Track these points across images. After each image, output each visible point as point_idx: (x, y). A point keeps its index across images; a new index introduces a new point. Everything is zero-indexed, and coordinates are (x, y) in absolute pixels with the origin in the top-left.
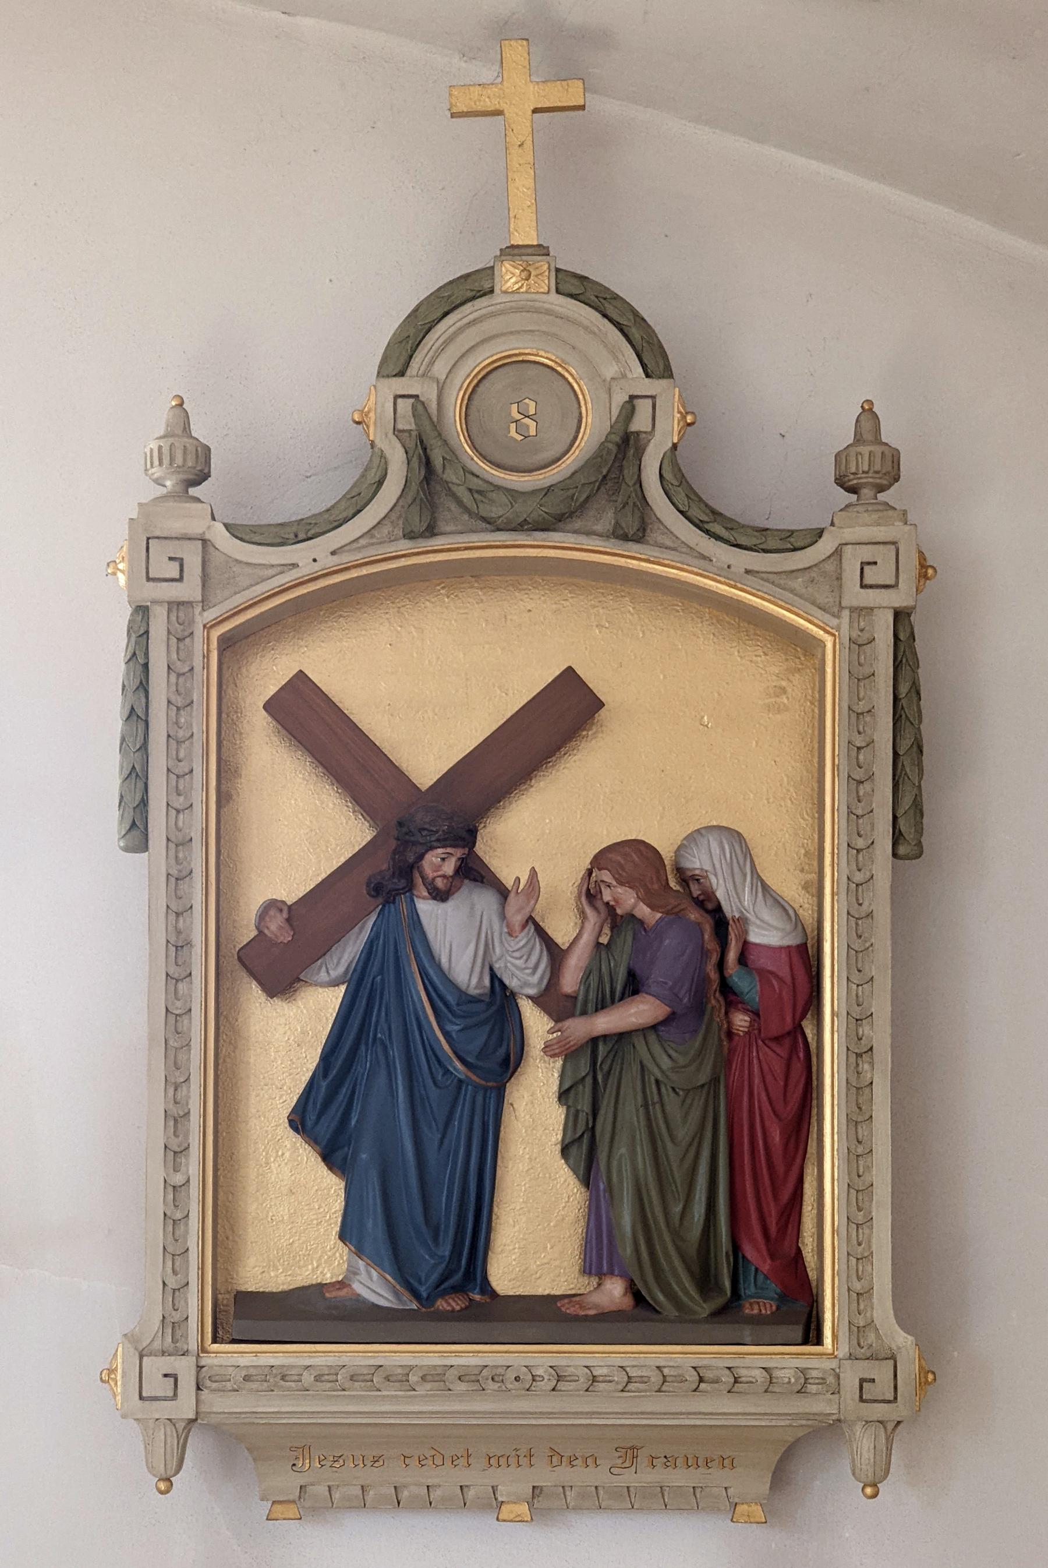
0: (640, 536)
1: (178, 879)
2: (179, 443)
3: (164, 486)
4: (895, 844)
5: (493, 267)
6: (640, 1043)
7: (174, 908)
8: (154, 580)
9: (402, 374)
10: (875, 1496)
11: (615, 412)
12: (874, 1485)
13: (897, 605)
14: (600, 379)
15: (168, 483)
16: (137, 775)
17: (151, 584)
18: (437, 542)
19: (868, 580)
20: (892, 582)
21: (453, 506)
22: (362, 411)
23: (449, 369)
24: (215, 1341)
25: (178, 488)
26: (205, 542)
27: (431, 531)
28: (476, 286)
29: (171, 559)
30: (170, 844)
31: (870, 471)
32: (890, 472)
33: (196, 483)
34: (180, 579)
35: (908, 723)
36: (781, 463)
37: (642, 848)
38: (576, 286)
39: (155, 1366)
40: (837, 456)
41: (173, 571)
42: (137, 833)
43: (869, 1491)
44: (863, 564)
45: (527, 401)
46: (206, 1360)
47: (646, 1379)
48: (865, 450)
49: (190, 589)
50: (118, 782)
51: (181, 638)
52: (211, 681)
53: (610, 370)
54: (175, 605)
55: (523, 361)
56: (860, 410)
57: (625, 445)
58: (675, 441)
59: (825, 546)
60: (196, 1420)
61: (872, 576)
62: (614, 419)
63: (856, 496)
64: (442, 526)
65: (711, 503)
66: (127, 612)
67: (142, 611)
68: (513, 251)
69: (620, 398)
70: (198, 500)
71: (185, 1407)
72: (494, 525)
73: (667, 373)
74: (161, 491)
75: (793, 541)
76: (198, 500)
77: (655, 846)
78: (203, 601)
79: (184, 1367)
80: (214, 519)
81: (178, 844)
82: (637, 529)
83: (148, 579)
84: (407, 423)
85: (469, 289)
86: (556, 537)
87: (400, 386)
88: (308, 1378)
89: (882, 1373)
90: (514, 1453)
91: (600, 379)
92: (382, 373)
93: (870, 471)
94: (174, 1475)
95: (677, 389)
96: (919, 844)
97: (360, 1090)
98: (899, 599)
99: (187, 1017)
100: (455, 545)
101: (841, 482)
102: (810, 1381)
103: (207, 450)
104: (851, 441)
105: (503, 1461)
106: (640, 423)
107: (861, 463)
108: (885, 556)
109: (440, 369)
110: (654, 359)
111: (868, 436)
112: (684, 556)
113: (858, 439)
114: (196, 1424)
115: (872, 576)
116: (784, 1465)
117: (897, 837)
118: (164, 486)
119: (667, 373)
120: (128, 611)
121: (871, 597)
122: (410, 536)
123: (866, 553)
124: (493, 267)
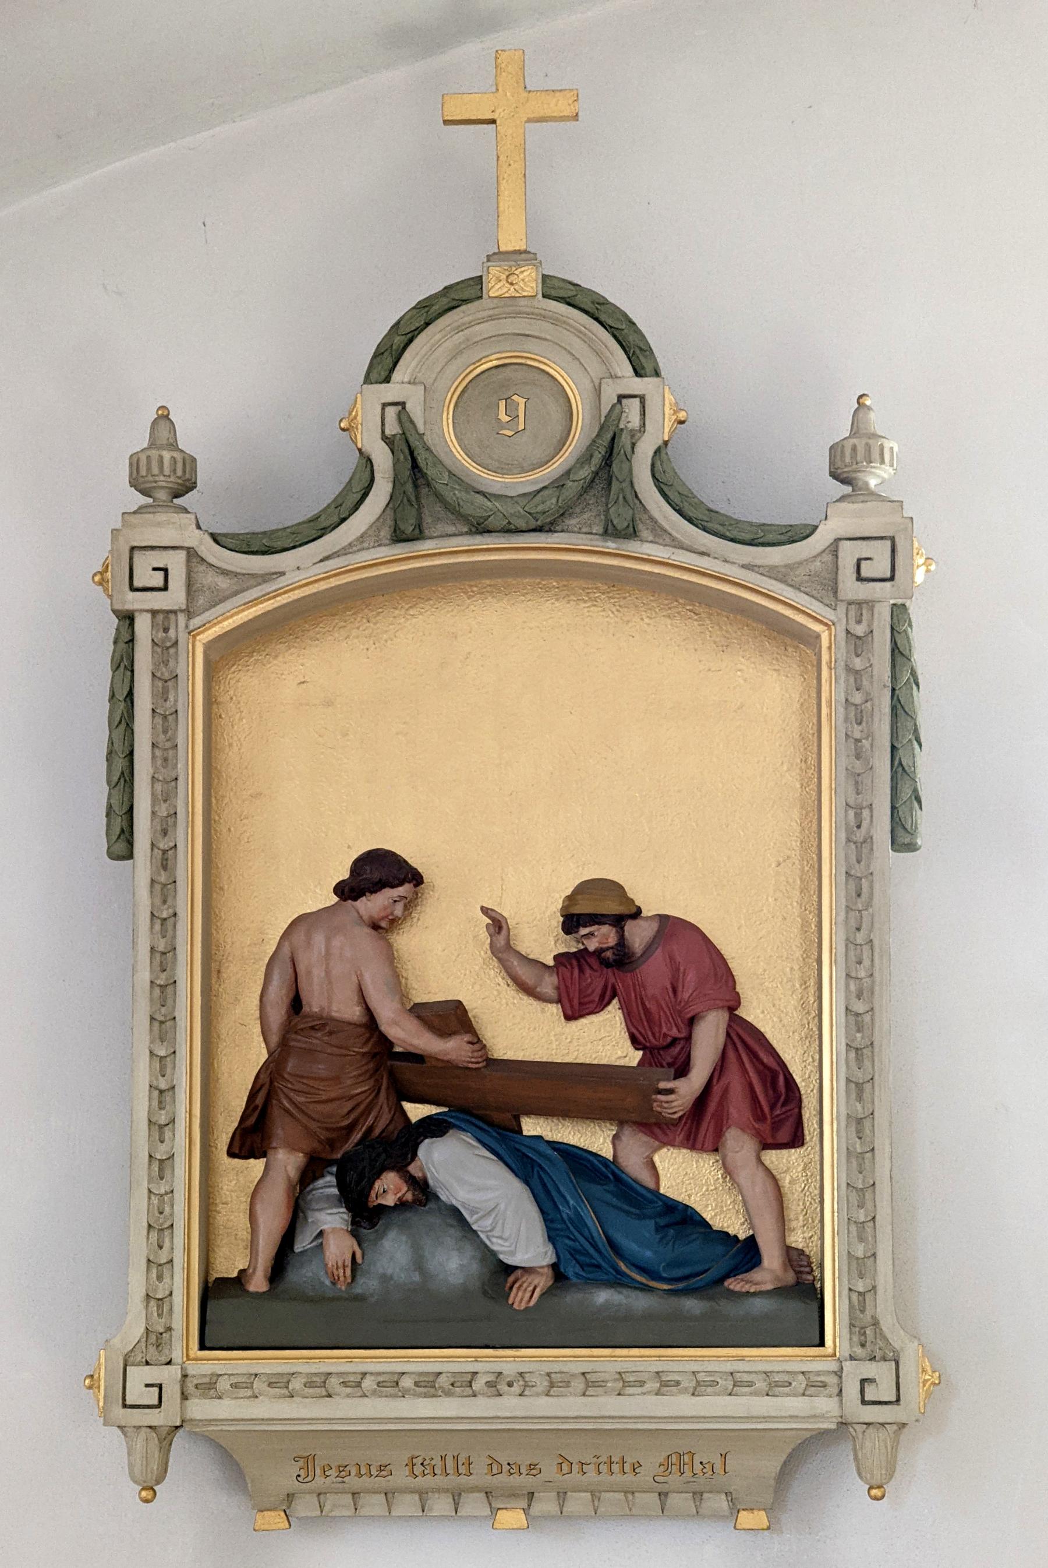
0: (631, 533)
1: (164, 889)
7: (161, 948)
14: (579, 373)
16: (125, 780)
18: (426, 546)
19: (864, 573)
21: (438, 508)
24: (203, 1347)
27: (418, 535)
29: (154, 569)
30: (156, 850)
34: (165, 588)
37: (714, 955)
39: (138, 1376)
40: (831, 448)
41: (158, 580)
42: (122, 842)
45: (515, 397)
49: (176, 597)
52: (195, 900)
54: (162, 618)
55: (543, 371)
56: (856, 406)
57: (610, 451)
58: (666, 438)
60: (181, 1426)
63: (850, 489)
68: (498, 256)
70: (186, 511)
73: (657, 374)
76: (186, 511)
77: (727, 950)
79: (168, 1376)
80: (199, 527)
81: (165, 860)
91: (579, 373)
92: (367, 380)
94: (158, 1483)
99: (171, 1093)
100: (444, 548)
103: (194, 460)
108: (880, 552)
110: (641, 359)
112: (672, 549)
113: (152, 445)
114: (181, 1431)
116: (784, 1474)
121: (864, 591)
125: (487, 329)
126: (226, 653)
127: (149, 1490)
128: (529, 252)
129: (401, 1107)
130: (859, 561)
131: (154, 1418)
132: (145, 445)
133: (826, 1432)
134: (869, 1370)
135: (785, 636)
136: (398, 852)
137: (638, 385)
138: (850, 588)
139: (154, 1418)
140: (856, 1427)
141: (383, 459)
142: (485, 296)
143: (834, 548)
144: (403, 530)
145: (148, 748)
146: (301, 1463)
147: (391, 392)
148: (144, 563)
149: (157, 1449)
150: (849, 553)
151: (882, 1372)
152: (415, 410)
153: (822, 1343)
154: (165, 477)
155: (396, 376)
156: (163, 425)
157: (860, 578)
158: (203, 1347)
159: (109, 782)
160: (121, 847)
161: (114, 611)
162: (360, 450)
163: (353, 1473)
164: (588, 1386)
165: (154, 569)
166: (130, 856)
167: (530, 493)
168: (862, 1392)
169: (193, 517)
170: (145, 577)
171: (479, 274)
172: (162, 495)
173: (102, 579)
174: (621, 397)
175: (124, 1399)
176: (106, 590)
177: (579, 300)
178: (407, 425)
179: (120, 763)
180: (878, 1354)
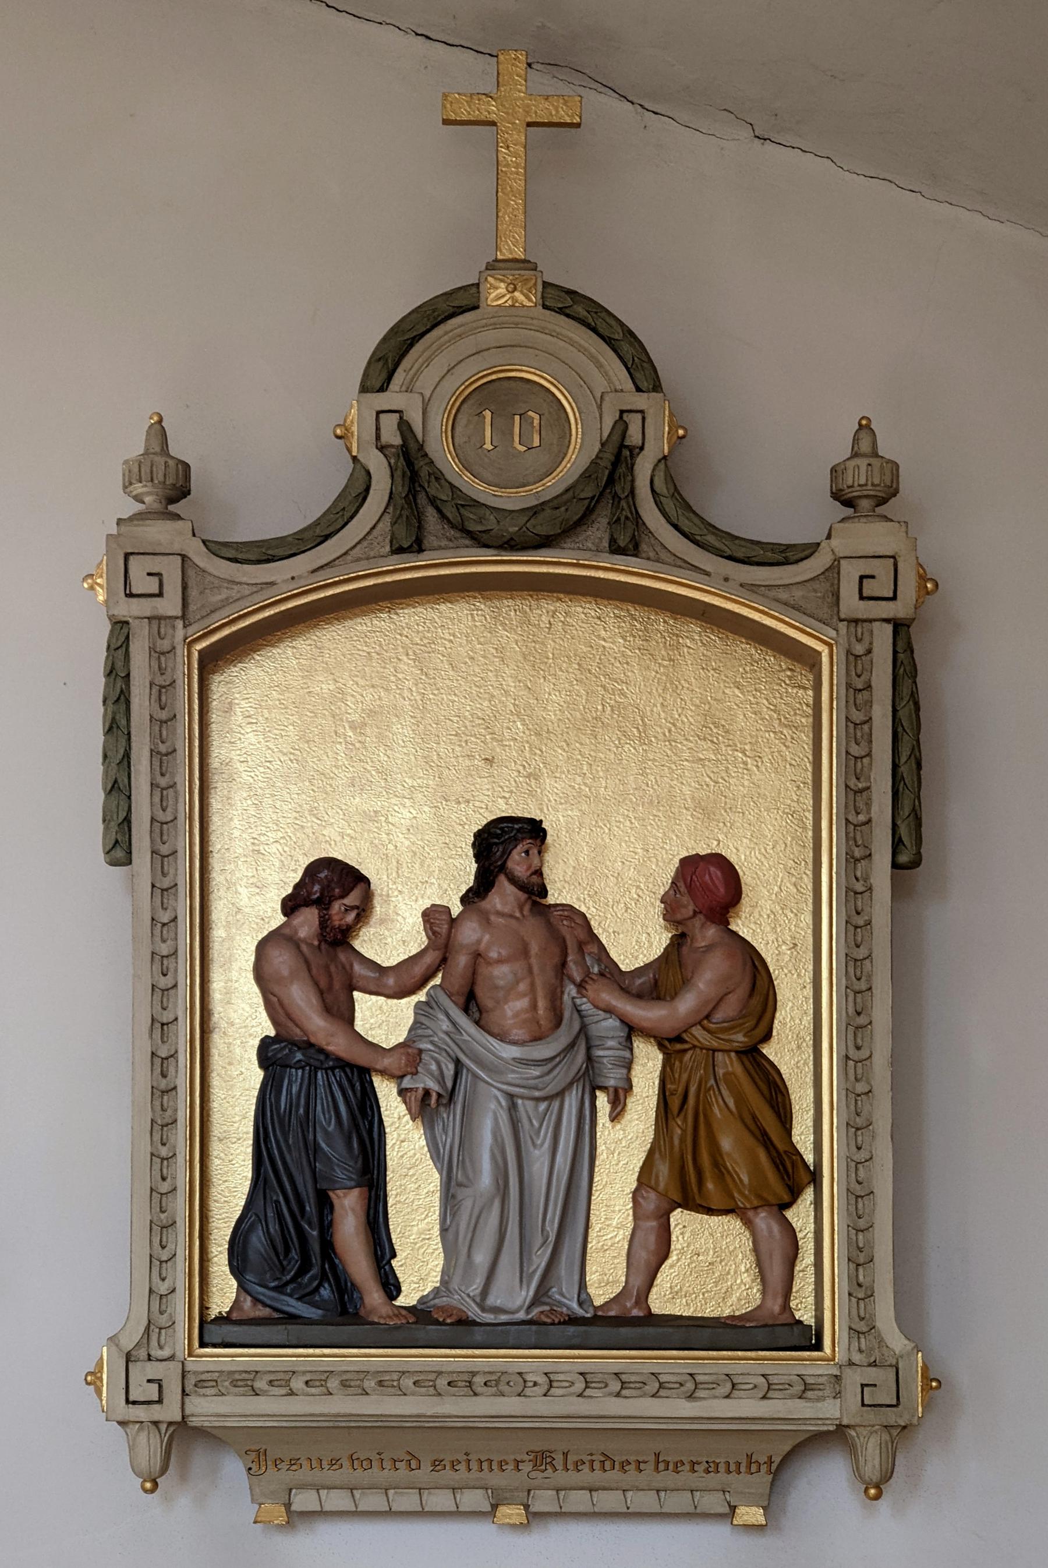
0: (633, 549)
2: (160, 460)
3: (143, 503)
4: (894, 854)
5: (478, 285)
6: (625, 1071)
9: (382, 389)
10: (877, 1497)
12: (877, 1487)
14: (582, 398)
15: (148, 499)
20: (894, 1402)
22: (344, 425)
23: (436, 379)
24: (202, 1345)
25: (157, 506)
26: (184, 557)
27: (418, 547)
28: (456, 303)
29: (149, 574)
31: (866, 490)
32: (886, 494)
33: (172, 500)
36: (771, 489)
38: (569, 304)
40: (834, 470)
41: (153, 586)
42: (119, 849)
43: (872, 1491)
44: (862, 578)
46: (192, 1364)
48: (863, 463)
49: (170, 605)
50: (102, 795)
51: (160, 655)
53: (600, 384)
54: (155, 619)
61: (869, 588)
62: (605, 435)
64: (430, 540)
66: (105, 628)
67: (121, 628)
71: (170, 1411)
72: (480, 540)
73: (657, 387)
74: (139, 507)
75: (786, 555)
78: (183, 617)
79: (170, 1374)
80: (194, 535)
81: (162, 858)
82: (629, 542)
83: (378, 413)
84: (391, 436)
85: (459, 303)
86: (544, 551)
87: (383, 401)
89: (883, 1377)
92: (364, 389)
93: (866, 490)
96: (919, 853)
97: (159, 1446)
98: (898, 610)
101: (836, 495)
103: (187, 467)
104: (848, 455)
105: (485, 1465)
106: (634, 436)
107: (859, 475)
108: (882, 570)
109: (426, 381)
110: (643, 371)
113: (855, 455)
115: (869, 588)
117: (897, 844)
118: (143, 503)
120: (107, 627)
122: (398, 550)
124: (478, 285)
125: (491, 337)
126: (212, 661)
128: (529, 261)
130: (862, 578)
131: (156, 1413)
133: (829, 1432)
134: (872, 1375)
136: (340, 858)
137: (641, 401)
138: (850, 603)
139: (156, 1413)
141: (377, 465)
142: (482, 304)
143: (834, 569)
145: (146, 753)
147: (391, 399)
148: (138, 568)
149: (178, 1444)
150: (850, 572)
152: (415, 418)
156: (864, 436)
159: (105, 789)
160: (119, 853)
164: (587, 1387)
166: (129, 862)
170: (141, 583)
174: (622, 412)
178: (409, 436)
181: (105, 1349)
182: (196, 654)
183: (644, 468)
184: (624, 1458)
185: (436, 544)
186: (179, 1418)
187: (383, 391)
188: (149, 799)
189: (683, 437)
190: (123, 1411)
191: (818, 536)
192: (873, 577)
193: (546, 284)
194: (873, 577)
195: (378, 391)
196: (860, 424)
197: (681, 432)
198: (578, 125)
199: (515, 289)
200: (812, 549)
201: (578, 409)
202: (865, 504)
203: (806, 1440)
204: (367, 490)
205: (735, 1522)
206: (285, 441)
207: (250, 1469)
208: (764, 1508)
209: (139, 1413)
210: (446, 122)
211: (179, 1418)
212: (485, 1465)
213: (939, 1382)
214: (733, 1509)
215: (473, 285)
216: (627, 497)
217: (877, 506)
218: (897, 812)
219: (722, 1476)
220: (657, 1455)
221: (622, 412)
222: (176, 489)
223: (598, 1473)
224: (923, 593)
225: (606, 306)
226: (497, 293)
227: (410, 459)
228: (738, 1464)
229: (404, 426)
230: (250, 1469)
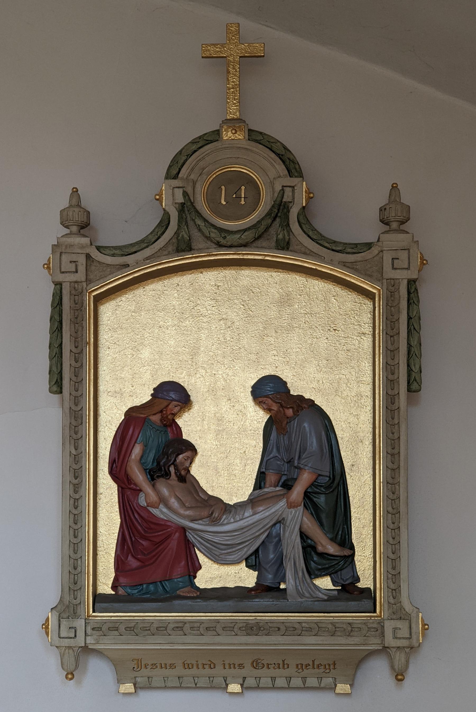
8: (63, 272)
11: (276, 195)
12: (72, 674)
13: (409, 277)
17: (63, 275)
24: (94, 611)
29: (71, 262)
31: (395, 216)
35: (415, 332)
36: (354, 218)
38: (255, 136)
42: (57, 385)
47: (128, 629)
49: (81, 276)
57: (280, 210)
59: (375, 250)
65: (422, 365)
67: (58, 285)
68: (227, 121)
69: (278, 188)
71: (80, 641)
73: (300, 175)
74: (67, 231)
82: (284, 246)
87: (175, 183)
88: (122, 628)
90: (223, 662)
91: (267, 175)
93: (395, 216)
95: (304, 183)
102: (337, 629)
105: (232, 666)
108: (403, 255)
110: (292, 167)
111: (74, 202)
119: (300, 175)
123: (394, 255)
126: (100, 299)
127: (70, 675)
129: (314, 585)
132: (67, 206)
134: (399, 624)
135: (369, 295)
140: (392, 649)
144: (184, 247)
146: (136, 662)
151: (403, 625)
152: (189, 190)
153: (375, 611)
154: (400, 676)
155: (180, 175)
157: (394, 268)
158: (94, 611)
161: (53, 282)
162: (164, 210)
163: (159, 667)
165: (71, 262)
167: (243, 230)
168: (393, 265)
169: (89, 239)
171: (218, 128)
172: (75, 229)
173: (47, 266)
174: (283, 186)
175: (59, 634)
176: (49, 272)
177: (275, 147)
179: (56, 350)
180: (403, 617)
181: (50, 614)
182: (92, 297)
183: (294, 212)
184: (307, 663)
185: (201, 246)
186: (83, 645)
187: (175, 179)
188: (70, 361)
189: (312, 198)
190: (57, 641)
191: (373, 239)
192: (398, 259)
193: (250, 130)
194: (398, 259)
195: (173, 179)
196: (392, 186)
197: (312, 195)
198: (263, 56)
199: (236, 133)
200: (369, 246)
201: (264, 184)
202: (394, 225)
203: (369, 654)
204: (169, 223)
205: (336, 692)
206: (130, 202)
207: (134, 668)
208: (241, 684)
209: (66, 642)
210: (203, 57)
211: (83, 645)
212: (232, 666)
213: (428, 625)
214: (227, 685)
215: (217, 130)
216: (414, 292)
217: (401, 224)
218: (403, 372)
219: (272, 670)
220: (283, 661)
221: (283, 186)
222: (84, 226)
223: (232, 669)
224: (309, 199)
225: (270, 134)
226: (227, 135)
227: (187, 208)
228: (329, 665)
229: (185, 194)
230: (134, 668)
